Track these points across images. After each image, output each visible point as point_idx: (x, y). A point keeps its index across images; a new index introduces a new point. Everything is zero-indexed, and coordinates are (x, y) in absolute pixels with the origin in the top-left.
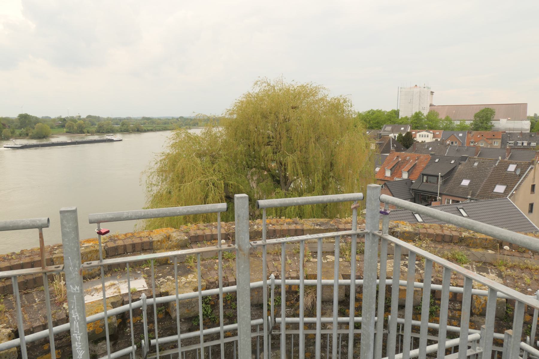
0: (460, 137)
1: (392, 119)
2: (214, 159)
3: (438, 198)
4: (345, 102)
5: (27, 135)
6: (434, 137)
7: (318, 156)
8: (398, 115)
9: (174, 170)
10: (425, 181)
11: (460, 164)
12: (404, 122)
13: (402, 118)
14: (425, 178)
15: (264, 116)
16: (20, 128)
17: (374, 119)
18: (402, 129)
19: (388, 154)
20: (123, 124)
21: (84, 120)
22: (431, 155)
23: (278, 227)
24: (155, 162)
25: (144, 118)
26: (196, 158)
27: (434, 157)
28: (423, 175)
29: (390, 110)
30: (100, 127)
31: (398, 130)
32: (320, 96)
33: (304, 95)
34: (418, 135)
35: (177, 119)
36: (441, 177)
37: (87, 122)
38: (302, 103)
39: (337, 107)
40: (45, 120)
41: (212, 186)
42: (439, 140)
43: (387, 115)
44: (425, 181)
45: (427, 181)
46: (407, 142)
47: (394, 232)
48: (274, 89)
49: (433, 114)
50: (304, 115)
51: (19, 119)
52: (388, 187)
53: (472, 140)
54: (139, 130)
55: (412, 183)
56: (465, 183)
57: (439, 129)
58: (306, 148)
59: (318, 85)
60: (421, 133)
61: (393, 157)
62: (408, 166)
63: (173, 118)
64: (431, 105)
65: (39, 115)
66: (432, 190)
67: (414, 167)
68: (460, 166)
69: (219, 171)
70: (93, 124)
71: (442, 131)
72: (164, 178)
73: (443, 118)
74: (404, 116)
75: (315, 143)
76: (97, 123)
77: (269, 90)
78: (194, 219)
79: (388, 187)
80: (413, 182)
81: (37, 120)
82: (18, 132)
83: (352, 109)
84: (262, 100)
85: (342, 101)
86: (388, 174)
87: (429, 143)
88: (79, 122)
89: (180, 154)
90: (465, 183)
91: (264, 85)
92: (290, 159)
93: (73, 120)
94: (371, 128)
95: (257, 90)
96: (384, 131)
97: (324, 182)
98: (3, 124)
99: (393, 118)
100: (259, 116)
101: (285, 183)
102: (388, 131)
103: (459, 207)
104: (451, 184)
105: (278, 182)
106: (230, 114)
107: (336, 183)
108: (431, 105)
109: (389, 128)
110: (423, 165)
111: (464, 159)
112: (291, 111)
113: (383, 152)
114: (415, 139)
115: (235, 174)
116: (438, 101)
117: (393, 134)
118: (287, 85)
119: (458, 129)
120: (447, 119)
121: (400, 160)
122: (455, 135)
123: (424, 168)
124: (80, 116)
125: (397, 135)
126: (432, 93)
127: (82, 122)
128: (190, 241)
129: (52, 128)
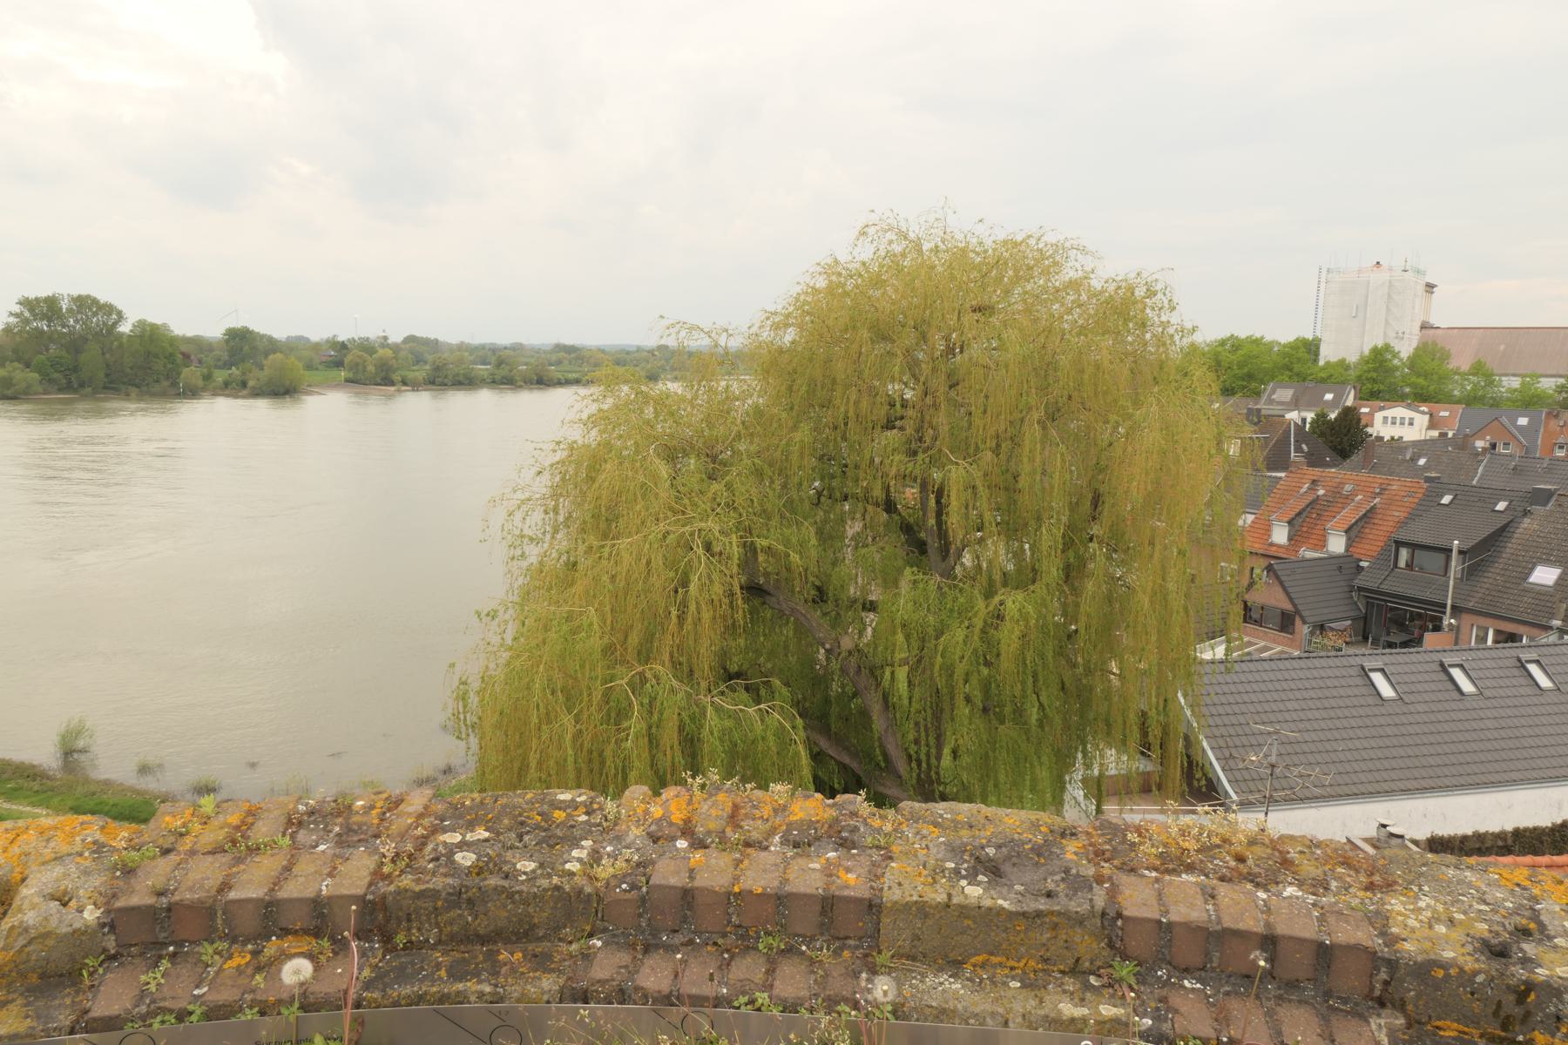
0: (1520, 429)
1: (1297, 368)
2: (715, 466)
3: (1448, 620)
4: (1151, 293)
5: (244, 384)
6: (1432, 426)
7: (1050, 470)
8: (1317, 354)
9: (593, 495)
10: (1402, 564)
11: (1526, 513)
12: (1336, 376)
13: (1328, 363)
14: (1404, 554)
15: (882, 334)
16: (228, 365)
17: (1241, 365)
18: (1329, 397)
19: (1283, 475)
20: (500, 364)
21: (396, 348)
22: (1428, 480)
23: (713, 871)
24: (535, 470)
25: (560, 348)
26: (657, 461)
27: (1436, 487)
28: (1399, 544)
29: (1291, 339)
30: (437, 369)
31: (1316, 401)
32: (1069, 273)
33: (1016, 271)
34: (1379, 416)
35: (651, 352)
36: (1460, 552)
37: (403, 354)
38: (1007, 292)
39: (1123, 309)
40: (293, 346)
41: (701, 551)
42: (1450, 435)
43: (1284, 355)
44: (1402, 564)
45: (1409, 566)
46: (1342, 439)
47: (1530, 986)
48: (920, 251)
49: (1431, 352)
50: (1012, 335)
51: (227, 341)
52: (1277, 577)
53: (1561, 440)
54: (541, 381)
55: (1360, 569)
56: (1545, 575)
57: (1450, 400)
58: (1015, 441)
59: (1062, 238)
60: (1390, 413)
61: (1302, 481)
62: (1349, 515)
63: (639, 349)
64: (1425, 326)
65: (280, 332)
66: (1427, 595)
67: (1368, 516)
68: (1527, 520)
69: (728, 505)
70: (419, 360)
71: (1460, 408)
72: (561, 518)
73: (1465, 367)
74: (1333, 359)
75: (1044, 428)
76: (430, 358)
77: (903, 255)
78: (639, 653)
79: (1277, 577)
80: (1363, 564)
81: (272, 346)
82: (220, 376)
83: (1174, 319)
84: (877, 282)
85: (1140, 292)
86: (1280, 535)
87: (1415, 443)
88: (381, 352)
89: (608, 446)
90: (1545, 575)
91: (890, 236)
92: (956, 475)
93: (366, 347)
94: (1228, 391)
95: (865, 252)
96: (1270, 401)
97: (1071, 553)
98: (183, 354)
99: (1299, 363)
100: (865, 334)
101: (945, 551)
102: (1282, 403)
103: (1524, 656)
104: (1493, 576)
105: (922, 547)
106: (776, 327)
107: (1109, 558)
108: (1425, 326)
109: (1285, 394)
110: (1399, 514)
111: (1542, 497)
112: (969, 318)
113: (1272, 467)
114: (1369, 430)
115: (782, 517)
116: (1448, 313)
117: (1301, 409)
118: (960, 236)
119: (1514, 401)
120: (1478, 369)
121: (1321, 492)
122: (1504, 420)
123: (1402, 524)
124: (385, 338)
125: (1310, 416)
126: (1430, 287)
127: (389, 353)
128: (111, 943)
129: (309, 367)
